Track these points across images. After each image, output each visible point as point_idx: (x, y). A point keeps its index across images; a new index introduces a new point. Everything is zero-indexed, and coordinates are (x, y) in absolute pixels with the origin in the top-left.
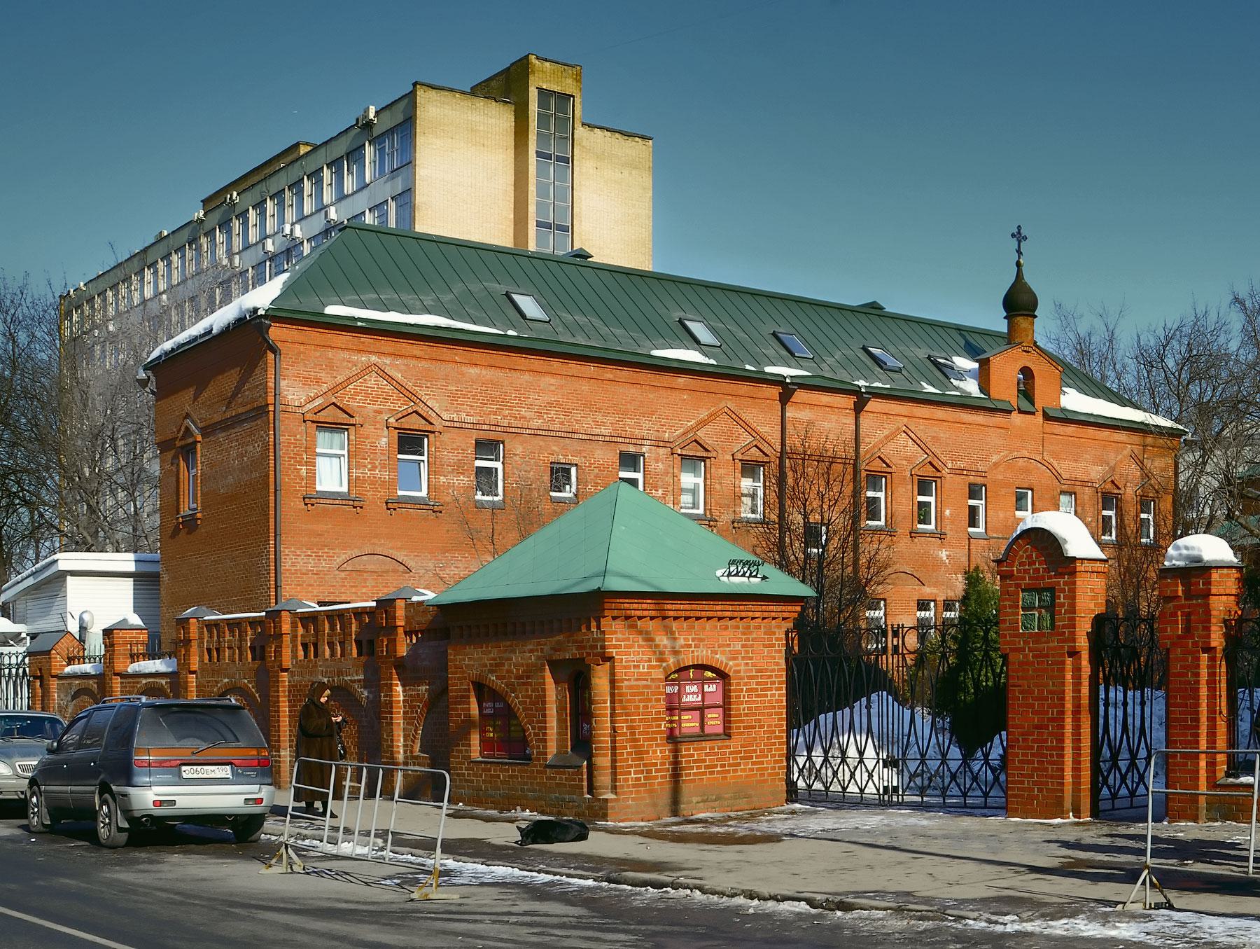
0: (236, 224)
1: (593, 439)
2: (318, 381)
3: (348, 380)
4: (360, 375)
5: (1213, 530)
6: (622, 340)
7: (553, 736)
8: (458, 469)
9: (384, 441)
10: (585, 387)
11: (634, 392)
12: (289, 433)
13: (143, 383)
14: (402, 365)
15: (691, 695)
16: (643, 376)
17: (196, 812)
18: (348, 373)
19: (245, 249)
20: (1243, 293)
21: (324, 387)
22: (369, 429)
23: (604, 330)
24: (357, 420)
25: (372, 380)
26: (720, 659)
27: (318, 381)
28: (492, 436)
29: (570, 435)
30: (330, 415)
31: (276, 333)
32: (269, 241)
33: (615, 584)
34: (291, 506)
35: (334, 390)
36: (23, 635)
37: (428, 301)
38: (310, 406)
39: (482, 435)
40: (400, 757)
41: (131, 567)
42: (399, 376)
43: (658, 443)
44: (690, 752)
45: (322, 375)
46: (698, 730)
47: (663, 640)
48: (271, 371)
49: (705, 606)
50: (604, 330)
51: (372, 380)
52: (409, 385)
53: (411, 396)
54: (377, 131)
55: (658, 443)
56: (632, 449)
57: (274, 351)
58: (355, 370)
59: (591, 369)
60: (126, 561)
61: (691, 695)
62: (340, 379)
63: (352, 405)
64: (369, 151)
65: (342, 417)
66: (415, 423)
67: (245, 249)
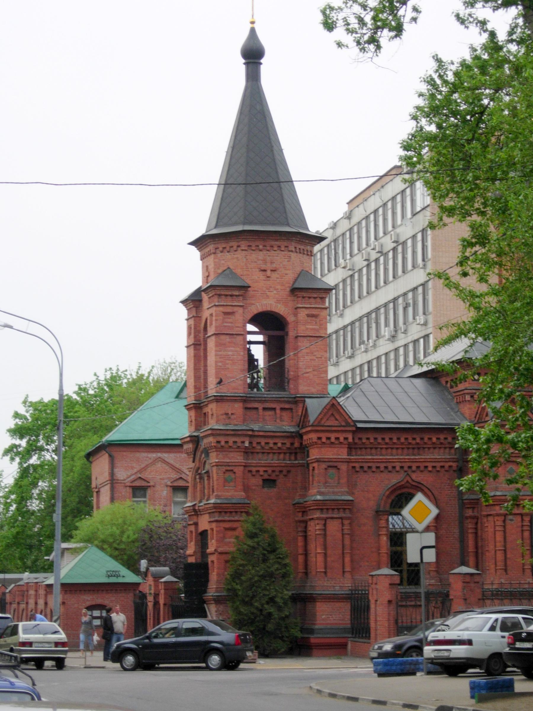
2: (132, 468)
3: (147, 466)
5: (455, 607)
9: (165, 492)
17: (233, 138)
18: (147, 463)
20: (249, 289)
21: (135, 470)
22: (158, 488)
24: (152, 484)
25: (159, 465)
27: (132, 468)
35: (140, 471)
36: (509, 498)
38: (129, 479)
40: (308, 327)
45: (134, 465)
46: (433, 550)
49: (362, 196)
52: (177, 466)
53: (179, 471)
58: (150, 461)
62: (143, 466)
65: (144, 484)
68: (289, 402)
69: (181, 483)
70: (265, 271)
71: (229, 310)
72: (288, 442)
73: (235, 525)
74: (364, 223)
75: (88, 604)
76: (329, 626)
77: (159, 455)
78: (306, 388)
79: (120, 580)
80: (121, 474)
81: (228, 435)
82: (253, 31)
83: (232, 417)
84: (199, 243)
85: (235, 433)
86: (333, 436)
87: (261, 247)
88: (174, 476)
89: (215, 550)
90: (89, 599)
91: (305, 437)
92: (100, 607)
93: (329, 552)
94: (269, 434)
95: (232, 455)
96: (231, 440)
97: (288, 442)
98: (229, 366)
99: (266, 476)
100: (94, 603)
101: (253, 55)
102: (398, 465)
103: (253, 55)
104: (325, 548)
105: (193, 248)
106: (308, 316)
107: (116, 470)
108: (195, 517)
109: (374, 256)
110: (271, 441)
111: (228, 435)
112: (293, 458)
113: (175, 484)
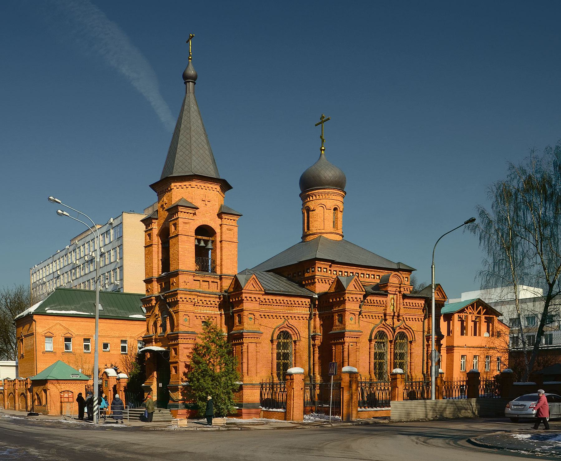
0: (77, 250)
1: (114, 337)
4: (55, 325)
6: (122, 313)
7: (44, 403)
8: (80, 345)
10: (111, 325)
11: (124, 325)
12: (39, 338)
13: (14, 324)
14: (66, 322)
15: (66, 395)
16: (127, 322)
19: (81, 258)
23: (118, 311)
25: (58, 326)
26: (71, 390)
27: (45, 327)
28: (88, 338)
29: (108, 336)
30: (48, 334)
31: (35, 317)
32: (86, 257)
33: (49, 378)
34: (39, 354)
35: (49, 329)
37: (73, 307)
39: (85, 337)
41: (15, 364)
42: (64, 325)
43: (131, 337)
44: (63, 405)
47: (59, 387)
48: (34, 325)
50: (118, 311)
51: (58, 326)
53: (67, 329)
54: (114, 226)
55: (131, 337)
56: (124, 339)
57: (35, 321)
59: (113, 321)
60: (13, 363)
61: (66, 395)
63: (53, 332)
64: (112, 231)
66: (68, 335)
67: (81, 258)
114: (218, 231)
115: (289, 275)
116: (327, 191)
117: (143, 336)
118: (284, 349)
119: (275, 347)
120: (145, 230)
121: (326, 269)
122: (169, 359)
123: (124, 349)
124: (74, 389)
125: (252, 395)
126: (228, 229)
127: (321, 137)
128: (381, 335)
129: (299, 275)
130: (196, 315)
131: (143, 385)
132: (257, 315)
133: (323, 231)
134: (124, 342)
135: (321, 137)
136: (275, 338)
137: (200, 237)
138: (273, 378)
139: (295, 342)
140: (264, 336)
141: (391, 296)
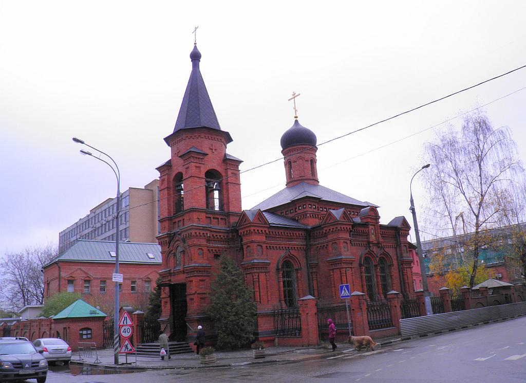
25: (79, 271)
26: (90, 326)
35: (71, 274)
43: (139, 279)
53: (86, 273)
55: (139, 279)
68: (225, 215)
69: (88, 279)
70: (212, 149)
71: (198, 165)
72: (226, 235)
73: (205, 278)
74: (100, 214)
75: (81, 328)
76: (264, 331)
77: (79, 267)
78: (233, 209)
79: (96, 315)
80: (63, 275)
81: (200, 229)
82: (195, 47)
83: (201, 220)
84: (168, 140)
85: (204, 228)
86: (260, 229)
87: (210, 138)
88: (85, 275)
89: (196, 292)
90: (82, 325)
91: (240, 231)
92: (87, 329)
93: (261, 291)
94: (217, 230)
95: (201, 240)
96: (202, 232)
97: (226, 235)
98: (198, 194)
99: (216, 253)
100: (84, 327)
101: (195, 57)
102: (284, 246)
103: (195, 57)
104: (259, 289)
105: (145, 157)
106: (232, 173)
107: (61, 273)
108: (169, 277)
109: (104, 223)
110: (218, 234)
111: (200, 229)
112: (227, 244)
113: (86, 279)
114: (223, 174)
115: (282, 213)
116: (304, 146)
117: (341, 175)
118: (288, 277)
119: (281, 275)
120: (159, 176)
121: (315, 205)
122: (186, 292)
123: (133, 289)
124: (93, 326)
125: (265, 326)
126: (232, 173)
127: (295, 108)
128: (367, 260)
129: (291, 213)
130: (209, 248)
131: (200, 327)
132: (264, 246)
133: (304, 178)
134: (134, 282)
135: (295, 108)
136: (280, 267)
137: (209, 180)
138: (281, 305)
139: (297, 270)
140: (271, 266)
141: (371, 227)
